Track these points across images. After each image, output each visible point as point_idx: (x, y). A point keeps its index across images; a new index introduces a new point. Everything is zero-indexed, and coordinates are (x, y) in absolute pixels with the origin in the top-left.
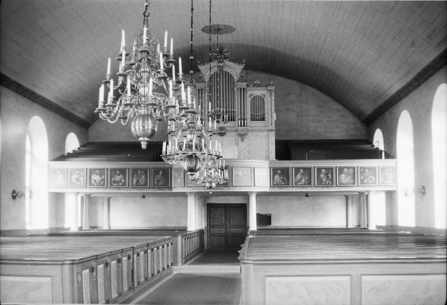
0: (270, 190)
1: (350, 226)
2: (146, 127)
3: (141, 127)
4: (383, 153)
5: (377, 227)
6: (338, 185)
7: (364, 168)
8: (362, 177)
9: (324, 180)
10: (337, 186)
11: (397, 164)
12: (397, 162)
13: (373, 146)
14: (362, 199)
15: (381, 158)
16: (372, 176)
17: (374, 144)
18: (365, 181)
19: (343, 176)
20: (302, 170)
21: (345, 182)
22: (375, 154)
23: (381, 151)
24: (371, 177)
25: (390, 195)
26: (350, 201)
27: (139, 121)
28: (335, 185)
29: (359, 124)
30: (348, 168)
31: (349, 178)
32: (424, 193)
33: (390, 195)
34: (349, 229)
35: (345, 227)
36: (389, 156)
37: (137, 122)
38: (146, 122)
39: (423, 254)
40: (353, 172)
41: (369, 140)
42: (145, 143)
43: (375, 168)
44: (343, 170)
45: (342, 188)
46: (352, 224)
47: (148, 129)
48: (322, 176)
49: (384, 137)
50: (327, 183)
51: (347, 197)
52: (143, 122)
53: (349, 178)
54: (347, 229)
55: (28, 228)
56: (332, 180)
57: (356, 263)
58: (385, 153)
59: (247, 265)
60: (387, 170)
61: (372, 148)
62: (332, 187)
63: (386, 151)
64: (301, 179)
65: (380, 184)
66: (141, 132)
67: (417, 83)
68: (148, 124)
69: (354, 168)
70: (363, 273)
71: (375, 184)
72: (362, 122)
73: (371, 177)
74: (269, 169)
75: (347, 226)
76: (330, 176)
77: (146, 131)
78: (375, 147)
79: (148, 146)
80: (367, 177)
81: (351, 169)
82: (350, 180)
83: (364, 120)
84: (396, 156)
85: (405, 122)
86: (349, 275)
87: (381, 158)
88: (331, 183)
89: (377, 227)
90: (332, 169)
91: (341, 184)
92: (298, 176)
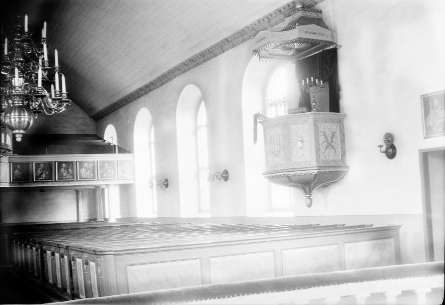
0: (10, 185)
1: (81, 220)
2: (22, 119)
3: (17, 120)
4: (117, 148)
5: (116, 219)
6: (57, 180)
7: (103, 162)
8: (102, 171)
9: (65, 174)
10: (56, 181)
11: (134, 159)
12: (134, 156)
13: (104, 141)
14: (94, 194)
15: (115, 153)
16: (111, 170)
17: (105, 138)
18: (105, 175)
19: (83, 170)
20: (42, 165)
21: (85, 177)
22: (107, 149)
23: (115, 146)
24: (110, 171)
25: (126, 189)
26: (80, 195)
27: (15, 113)
28: (117, 178)
29: (88, 120)
30: (88, 162)
31: (89, 172)
32: (167, 186)
33: (126, 189)
34: (79, 223)
35: (76, 221)
36: (122, 150)
37: (12, 114)
38: (22, 114)
39: (129, 245)
40: (93, 166)
41: (98, 135)
42: (21, 136)
43: (114, 162)
44: (83, 164)
45: (83, 182)
46: (84, 218)
47: (25, 121)
48: (62, 170)
49: (117, 132)
50: (68, 177)
51: (77, 192)
52: (20, 115)
53: (89, 172)
54: (78, 223)
55: (138, 217)
56: (73, 175)
57: (317, 237)
58: (119, 148)
59: (106, 257)
60: (106, 165)
61: (103, 143)
62: (73, 181)
63: (119, 146)
64: (42, 174)
65: (119, 178)
66: (17, 124)
67: (160, 83)
68: (24, 115)
69: (94, 162)
70: (128, 263)
71: (94, 178)
72: (91, 118)
73: (110, 171)
74: (8, 164)
75: (78, 220)
76: (70, 170)
77: (22, 123)
78: (106, 142)
79: (22, 138)
80: (106, 172)
81: (91, 164)
82: (90, 174)
83: (94, 116)
84: (133, 150)
85: (142, 119)
86: (273, 251)
87: (115, 153)
88: (71, 177)
89: (116, 219)
90: (72, 163)
91: (82, 178)
92: (39, 170)
